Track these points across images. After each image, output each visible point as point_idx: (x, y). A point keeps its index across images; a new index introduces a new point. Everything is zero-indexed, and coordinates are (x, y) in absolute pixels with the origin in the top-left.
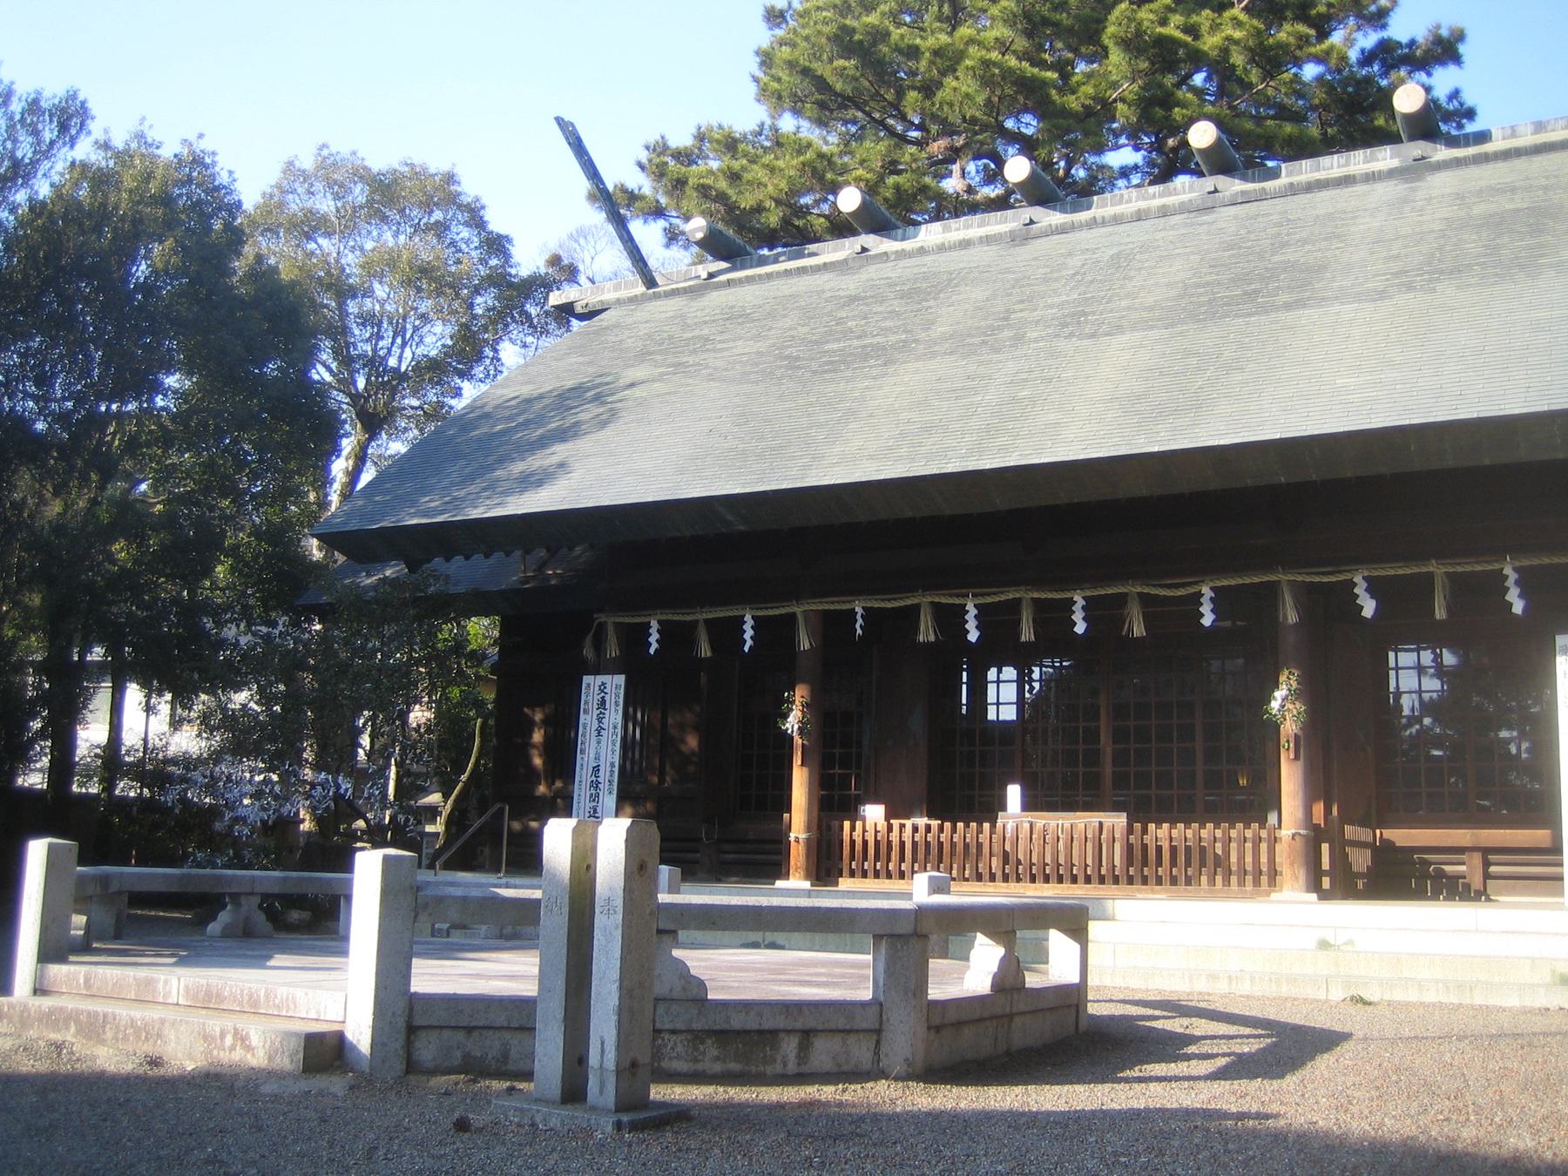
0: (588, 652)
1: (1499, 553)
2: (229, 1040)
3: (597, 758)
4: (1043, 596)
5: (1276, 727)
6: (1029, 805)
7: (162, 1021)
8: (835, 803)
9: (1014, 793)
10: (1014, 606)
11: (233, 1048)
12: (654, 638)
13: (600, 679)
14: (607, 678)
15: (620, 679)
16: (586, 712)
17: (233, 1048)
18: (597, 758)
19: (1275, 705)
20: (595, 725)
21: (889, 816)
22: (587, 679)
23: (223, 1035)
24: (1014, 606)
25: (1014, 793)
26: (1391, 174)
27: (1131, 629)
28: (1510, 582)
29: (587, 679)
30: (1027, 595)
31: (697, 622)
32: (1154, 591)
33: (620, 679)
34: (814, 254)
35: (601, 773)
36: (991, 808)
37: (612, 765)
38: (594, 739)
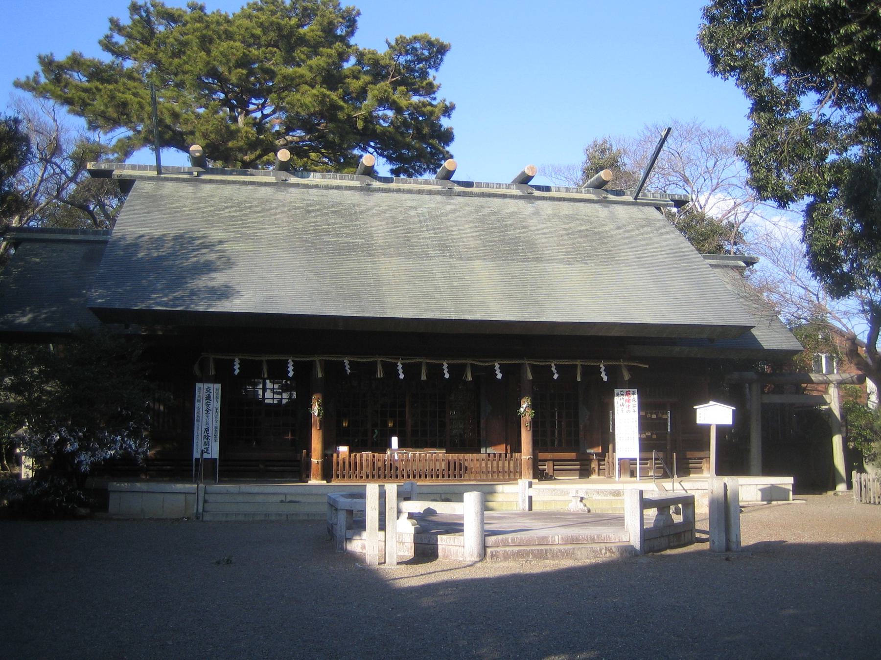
0: (196, 370)
1: (599, 359)
2: (603, 551)
3: (207, 424)
4: (431, 361)
5: (519, 418)
6: (401, 445)
7: (574, 549)
8: (329, 445)
9: (395, 441)
10: (419, 365)
11: (606, 553)
12: (291, 368)
13: (206, 385)
14: (211, 385)
15: (218, 386)
16: (199, 401)
17: (606, 553)
18: (207, 424)
19: (522, 410)
20: (205, 407)
21: (350, 452)
22: (198, 385)
23: (601, 550)
24: (419, 365)
25: (395, 441)
26: (439, 193)
27: (466, 377)
28: (602, 370)
29: (198, 385)
30: (379, 359)
31: (262, 361)
32: (476, 363)
33: (218, 386)
34: (251, 175)
35: (210, 431)
36: (385, 445)
37: (216, 428)
38: (204, 415)
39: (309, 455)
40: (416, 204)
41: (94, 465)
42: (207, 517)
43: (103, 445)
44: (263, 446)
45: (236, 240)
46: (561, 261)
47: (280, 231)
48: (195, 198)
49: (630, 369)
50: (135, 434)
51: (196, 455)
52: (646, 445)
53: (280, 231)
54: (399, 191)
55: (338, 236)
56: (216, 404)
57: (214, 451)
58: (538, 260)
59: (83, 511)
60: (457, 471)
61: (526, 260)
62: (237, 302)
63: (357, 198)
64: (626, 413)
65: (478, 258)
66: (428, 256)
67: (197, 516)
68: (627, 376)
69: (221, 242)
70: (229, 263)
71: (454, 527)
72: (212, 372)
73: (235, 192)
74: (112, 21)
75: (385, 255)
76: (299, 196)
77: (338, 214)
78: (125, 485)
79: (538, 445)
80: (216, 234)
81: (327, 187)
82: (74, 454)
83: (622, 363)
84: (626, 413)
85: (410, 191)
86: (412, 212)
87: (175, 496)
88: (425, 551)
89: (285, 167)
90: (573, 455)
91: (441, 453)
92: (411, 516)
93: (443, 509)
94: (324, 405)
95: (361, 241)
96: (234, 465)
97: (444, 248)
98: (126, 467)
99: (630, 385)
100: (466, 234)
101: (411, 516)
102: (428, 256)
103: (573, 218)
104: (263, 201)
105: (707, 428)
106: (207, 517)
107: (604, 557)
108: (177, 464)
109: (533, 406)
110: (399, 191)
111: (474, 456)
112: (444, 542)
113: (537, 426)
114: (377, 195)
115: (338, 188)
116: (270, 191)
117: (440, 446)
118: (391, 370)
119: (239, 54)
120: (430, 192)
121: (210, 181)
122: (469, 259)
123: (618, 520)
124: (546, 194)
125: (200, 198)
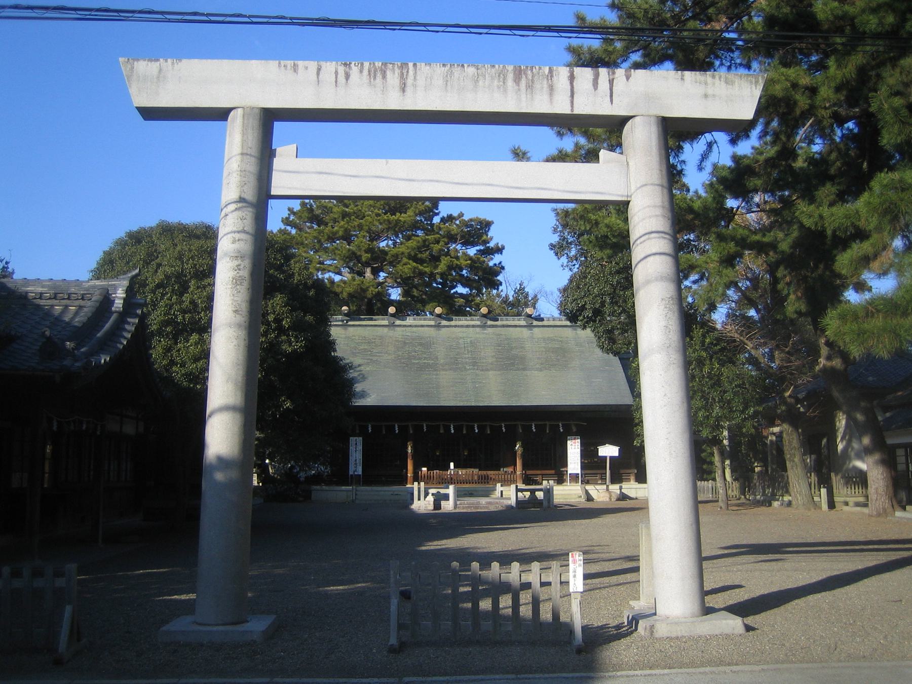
8: (417, 468)
9: (452, 465)
25: (452, 465)
26: (478, 326)
39: (407, 473)
40: (465, 335)
41: (306, 478)
42: (357, 502)
43: (310, 469)
44: (386, 468)
45: (368, 364)
46: (537, 369)
47: (390, 357)
48: (346, 338)
49: (576, 425)
50: (323, 464)
51: (351, 473)
52: (583, 467)
53: (390, 357)
54: (455, 326)
55: (420, 359)
56: (360, 447)
57: (360, 471)
58: (524, 369)
59: (301, 499)
60: (485, 480)
61: (518, 369)
62: (369, 400)
63: (432, 332)
64: (574, 449)
65: (492, 369)
66: (466, 369)
67: (353, 501)
68: (574, 429)
69: (359, 365)
70: (364, 378)
71: (446, 497)
72: (358, 431)
73: (367, 332)
74: (289, 209)
75: (443, 370)
76: (401, 333)
77: (421, 344)
78: (318, 487)
79: (525, 466)
80: (357, 361)
81: (416, 326)
82: (298, 473)
83: (571, 422)
84: (574, 449)
85: (462, 326)
86: (461, 341)
87: (344, 492)
88: (437, 506)
89: (393, 315)
90: (553, 472)
91: (476, 471)
92: (433, 494)
93: (443, 491)
94: (413, 448)
95: (431, 362)
96: (368, 478)
97: (474, 364)
98: (318, 479)
99: (575, 435)
100: (488, 354)
101: (433, 494)
102: (466, 369)
103: (551, 340)
104: (381, 337)
105: (604, 458)
106: (357, 502)
107: (500, 508)
108: (341, 476)
109: (522, 446)
110: (455, 326)
111: (497, 472)
112: (443, 503)
113: (523, 457)
114: (444, 330)
115: (422, 326)
116: (386, 330)
117: (475, 467)
118: (447, 429)
119: (366, 246)
120: (473, 326)
121: (353, 325)
122: (487, 370)
123: (510, 499)
124: (540, 323)
125: (349, 338)
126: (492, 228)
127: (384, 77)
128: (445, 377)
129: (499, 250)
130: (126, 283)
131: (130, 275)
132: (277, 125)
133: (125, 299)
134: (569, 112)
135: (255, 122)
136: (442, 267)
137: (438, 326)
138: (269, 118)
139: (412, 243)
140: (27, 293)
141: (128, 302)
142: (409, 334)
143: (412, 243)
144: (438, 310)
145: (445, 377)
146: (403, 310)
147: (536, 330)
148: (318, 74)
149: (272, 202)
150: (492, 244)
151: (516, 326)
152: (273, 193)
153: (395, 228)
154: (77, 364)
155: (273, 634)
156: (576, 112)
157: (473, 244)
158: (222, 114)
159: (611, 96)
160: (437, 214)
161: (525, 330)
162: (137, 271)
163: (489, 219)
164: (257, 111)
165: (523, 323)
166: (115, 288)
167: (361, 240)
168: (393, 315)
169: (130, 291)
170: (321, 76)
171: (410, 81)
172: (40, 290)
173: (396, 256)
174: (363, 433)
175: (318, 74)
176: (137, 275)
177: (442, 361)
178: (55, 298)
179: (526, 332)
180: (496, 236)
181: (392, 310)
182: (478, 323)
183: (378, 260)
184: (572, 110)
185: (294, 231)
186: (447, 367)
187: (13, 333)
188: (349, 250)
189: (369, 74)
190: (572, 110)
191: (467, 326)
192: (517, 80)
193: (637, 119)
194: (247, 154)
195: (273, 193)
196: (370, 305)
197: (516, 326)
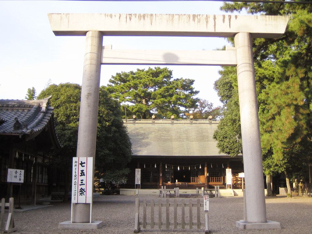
26: (189, 123)
40: (183, 127)
54: (180, 123)
56: (140, 173)
58: (208, 141)
77: (165, 131)
81: (163, 123)
85: (182, 123)
89: (154, 119)
110: (180, 123)
115: (166, 123)
116: (151, 125)
120: (187, 123)
121: (138, 123)
122: (193, 141)
126: (195, 82)
127: (144, 19)
128: (175, 144)
129: (197, 92)
130: (47, 101)
131: (48, 98)
132: (105, 38)
133: (46, 107)
134: (214, 32)
135: (97, 34)
136: (174, 98)
137: (172, 123)
138: (102, 34)
139: (162, 89)
140: (8, 104)
141: (47, 108)
142: (160, 127)
143: (162, 89)
144: (173, 117)
145: (175, 144)
146: (158, 117)
147: (213, 125)
148: (120, 18)
149: (102, 66)
150: (194, 90)
151: (204, 123)
152: (104, 61)
153: (156, 84)
154: (28, 131)
155: (100, 227)
156: (216, 32)
157: (187, 90)
158: (84, 33)
159: (230, 25)
160: (172, 77)
161: (208, 125)
162: (51, 96)
163: (191, 78)
164: (97, 32)
165: (208, 122)
166: (42, 103)
167: (141, 88)
168: (154, 119)
169: (48, 104)
170: (120, 19)
171: (154, 21)
172: (13, 104)
173: (155, 95)
174: (141, 167)
175: (120, 18)
176: (51, 98)
177: (174, 138)
178: (19, 107)
179: (209, 126)
180: (195, 87)
181: (153, 117)
182: (189, 122)
183: (148, 96)
184: (215, 31)
185: (113, 85)
186: (176, 140)
187: (3, 119)
188: (136, 92)
189: (139, 17)
190: (215, 31)
191: (185, 123)
192: (194, 20)
193: (239, 34)
194: (94, 53)
195: (103, 62)
196: (145, 115)
197: (204, 123)
